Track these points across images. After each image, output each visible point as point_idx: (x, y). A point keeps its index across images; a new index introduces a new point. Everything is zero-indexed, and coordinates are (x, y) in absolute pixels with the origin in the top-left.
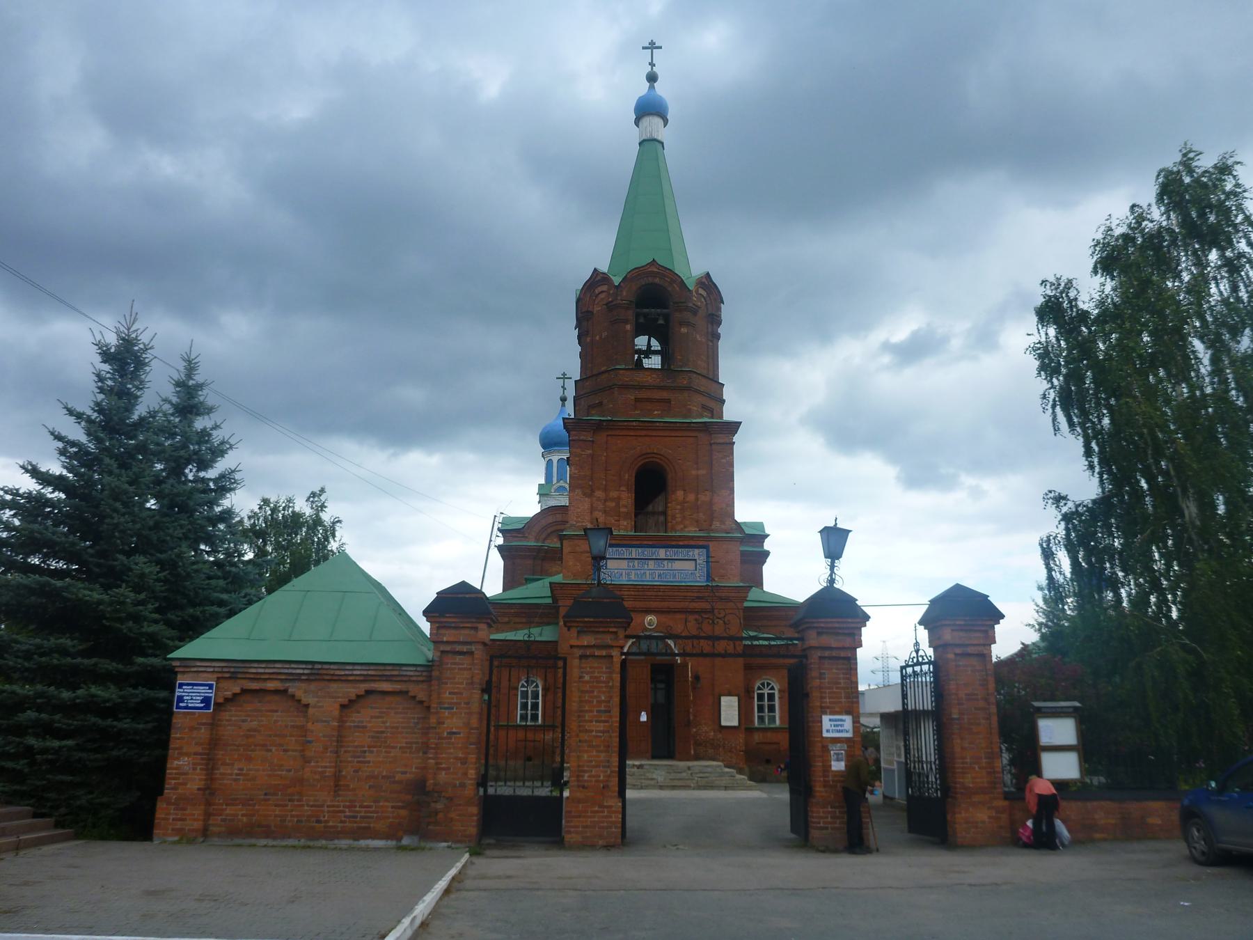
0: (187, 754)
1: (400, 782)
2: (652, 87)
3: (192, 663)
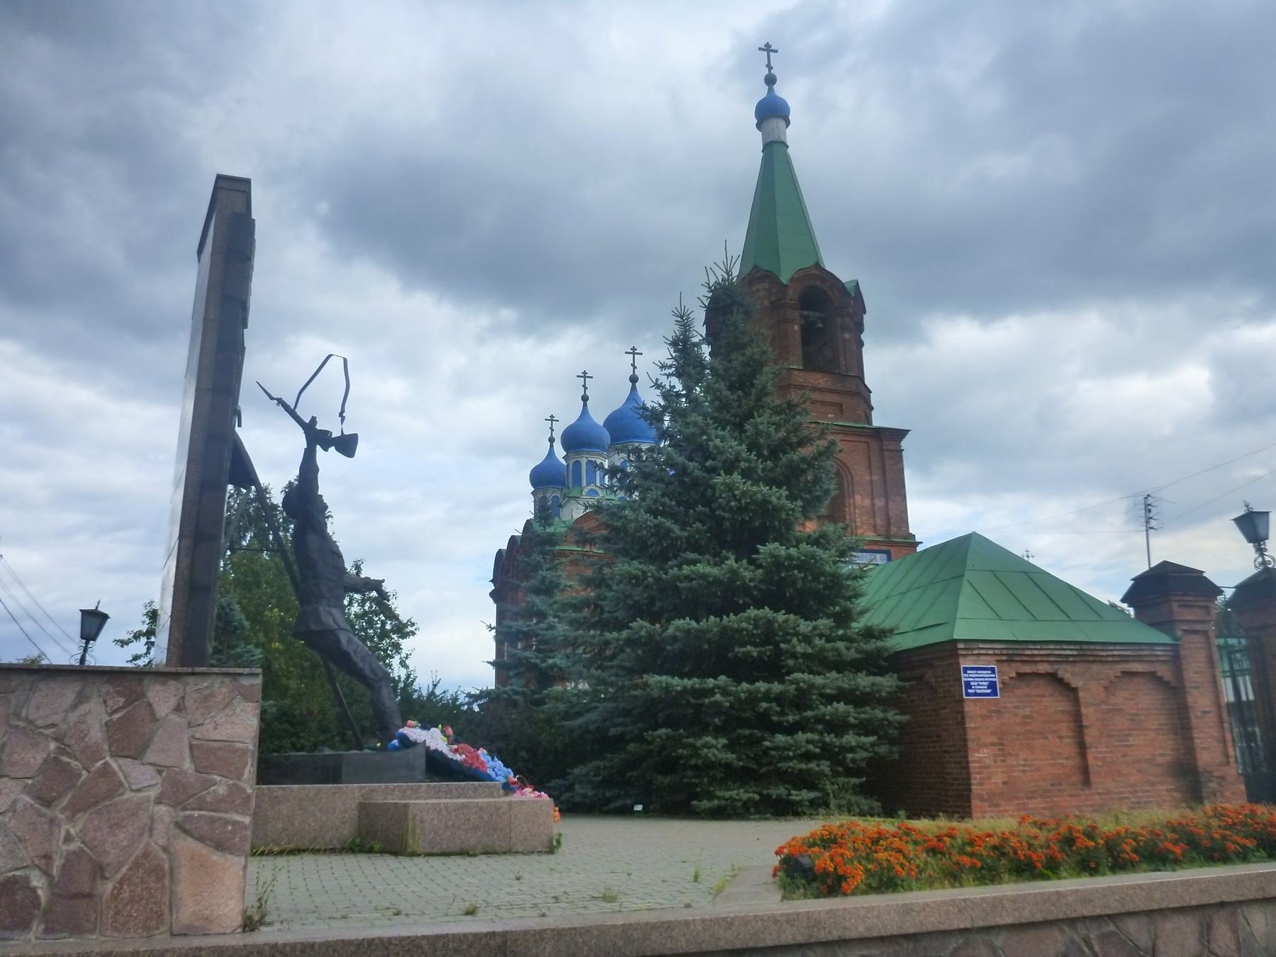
0: (985, 745)
1: (1159, 765)
2: (771, 90)
3: (975, 646)
